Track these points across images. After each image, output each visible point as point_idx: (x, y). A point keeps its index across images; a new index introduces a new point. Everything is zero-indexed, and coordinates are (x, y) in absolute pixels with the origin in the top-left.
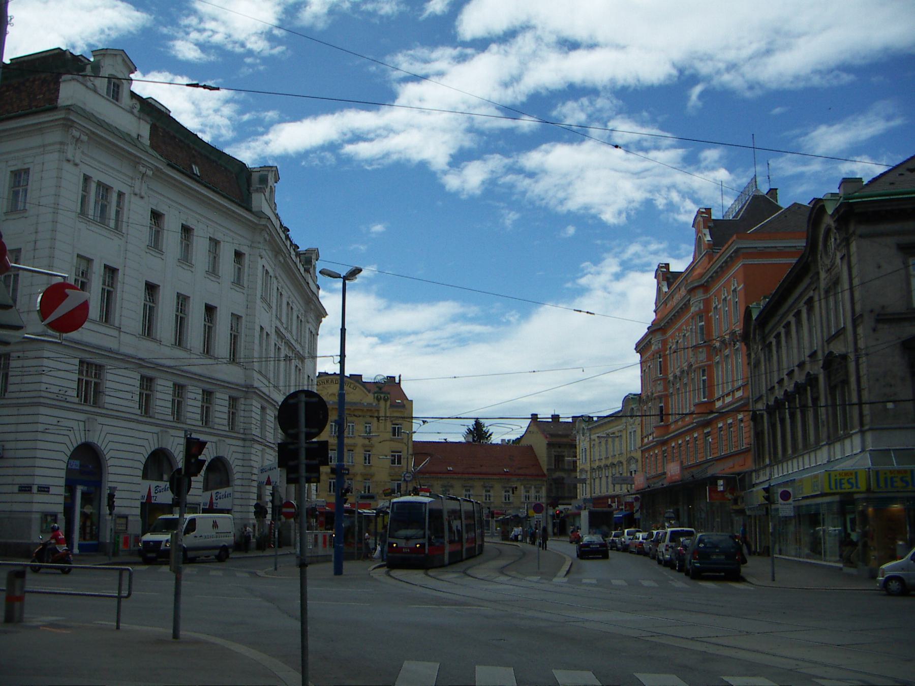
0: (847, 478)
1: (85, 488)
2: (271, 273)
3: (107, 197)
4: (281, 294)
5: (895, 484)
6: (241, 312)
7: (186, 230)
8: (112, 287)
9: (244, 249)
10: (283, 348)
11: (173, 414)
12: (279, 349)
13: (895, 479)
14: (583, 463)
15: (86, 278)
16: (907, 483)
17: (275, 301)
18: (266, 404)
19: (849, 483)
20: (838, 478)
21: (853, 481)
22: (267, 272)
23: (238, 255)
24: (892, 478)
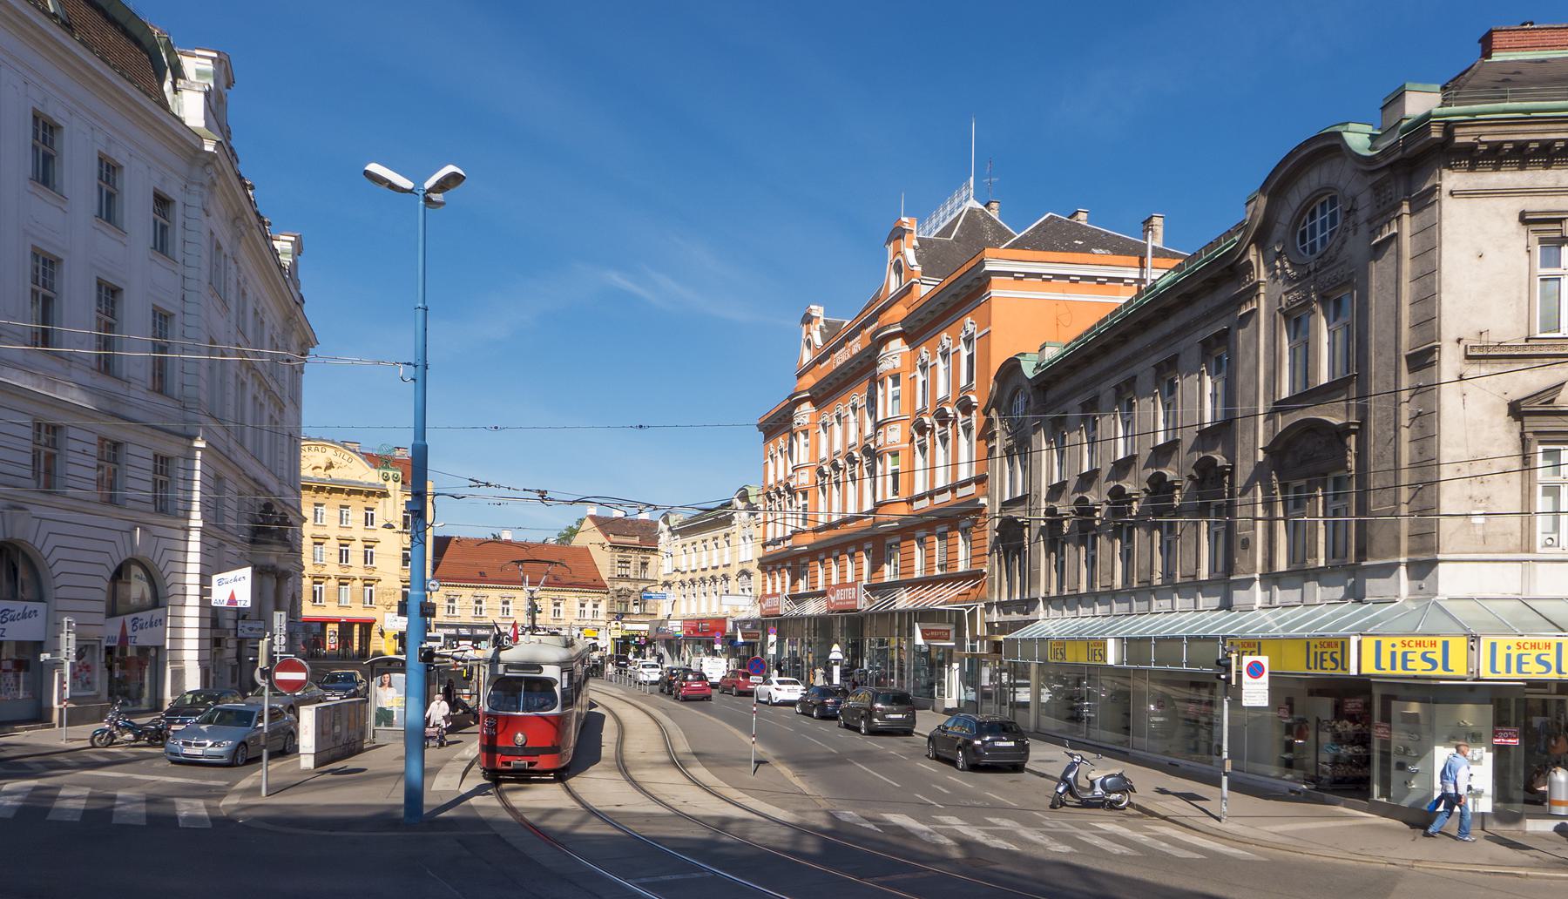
0: (1330, 650)
1: (1310, 563)
2: (226, 249)
3: (52, 141)
4: (244, 294)
5: (1410, 665)
6: (171, 304)
7: (109, 170)
8: (113, 316)
9: (173, 190)
10: (249, 383)
11: (36, 474)
12: (243, 384)
13: (1524, 659)
14: (1446, 506)
15: (113, 316)
16: (1434, 664)
17: (234, 300)
18: (225, 472)
19: (1333, 659)
20: (1319, 650)
21: (1338, 656)
22: (219, 247)
23: (162, 202)
24: (1520, 657)
